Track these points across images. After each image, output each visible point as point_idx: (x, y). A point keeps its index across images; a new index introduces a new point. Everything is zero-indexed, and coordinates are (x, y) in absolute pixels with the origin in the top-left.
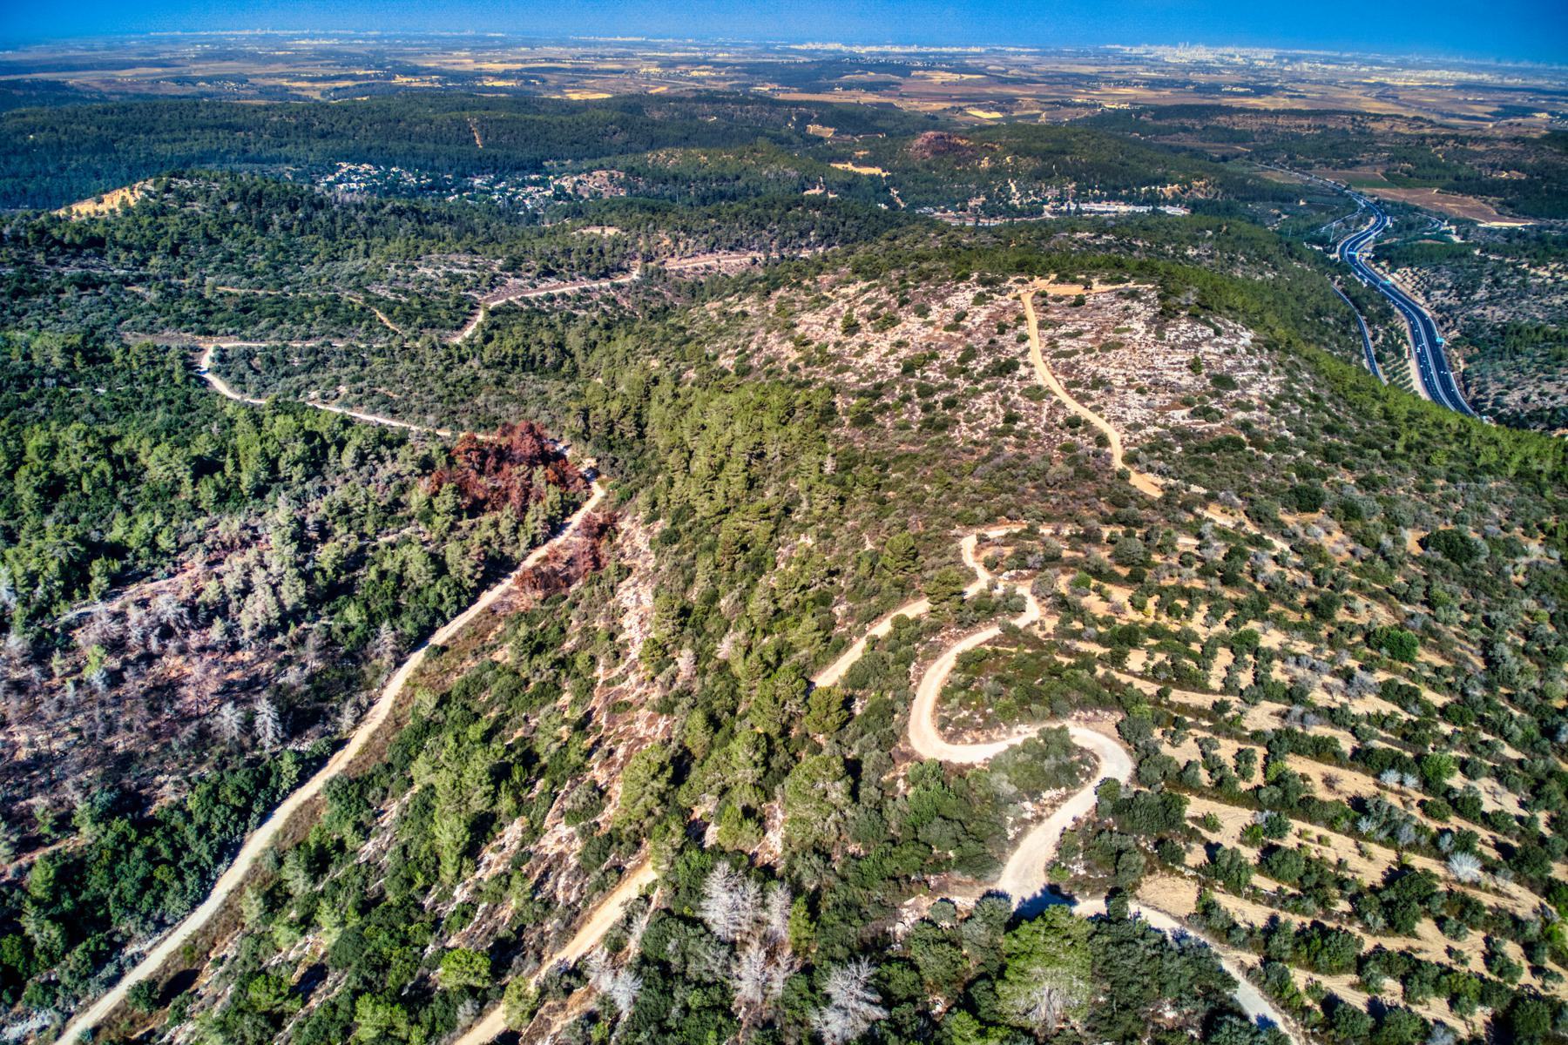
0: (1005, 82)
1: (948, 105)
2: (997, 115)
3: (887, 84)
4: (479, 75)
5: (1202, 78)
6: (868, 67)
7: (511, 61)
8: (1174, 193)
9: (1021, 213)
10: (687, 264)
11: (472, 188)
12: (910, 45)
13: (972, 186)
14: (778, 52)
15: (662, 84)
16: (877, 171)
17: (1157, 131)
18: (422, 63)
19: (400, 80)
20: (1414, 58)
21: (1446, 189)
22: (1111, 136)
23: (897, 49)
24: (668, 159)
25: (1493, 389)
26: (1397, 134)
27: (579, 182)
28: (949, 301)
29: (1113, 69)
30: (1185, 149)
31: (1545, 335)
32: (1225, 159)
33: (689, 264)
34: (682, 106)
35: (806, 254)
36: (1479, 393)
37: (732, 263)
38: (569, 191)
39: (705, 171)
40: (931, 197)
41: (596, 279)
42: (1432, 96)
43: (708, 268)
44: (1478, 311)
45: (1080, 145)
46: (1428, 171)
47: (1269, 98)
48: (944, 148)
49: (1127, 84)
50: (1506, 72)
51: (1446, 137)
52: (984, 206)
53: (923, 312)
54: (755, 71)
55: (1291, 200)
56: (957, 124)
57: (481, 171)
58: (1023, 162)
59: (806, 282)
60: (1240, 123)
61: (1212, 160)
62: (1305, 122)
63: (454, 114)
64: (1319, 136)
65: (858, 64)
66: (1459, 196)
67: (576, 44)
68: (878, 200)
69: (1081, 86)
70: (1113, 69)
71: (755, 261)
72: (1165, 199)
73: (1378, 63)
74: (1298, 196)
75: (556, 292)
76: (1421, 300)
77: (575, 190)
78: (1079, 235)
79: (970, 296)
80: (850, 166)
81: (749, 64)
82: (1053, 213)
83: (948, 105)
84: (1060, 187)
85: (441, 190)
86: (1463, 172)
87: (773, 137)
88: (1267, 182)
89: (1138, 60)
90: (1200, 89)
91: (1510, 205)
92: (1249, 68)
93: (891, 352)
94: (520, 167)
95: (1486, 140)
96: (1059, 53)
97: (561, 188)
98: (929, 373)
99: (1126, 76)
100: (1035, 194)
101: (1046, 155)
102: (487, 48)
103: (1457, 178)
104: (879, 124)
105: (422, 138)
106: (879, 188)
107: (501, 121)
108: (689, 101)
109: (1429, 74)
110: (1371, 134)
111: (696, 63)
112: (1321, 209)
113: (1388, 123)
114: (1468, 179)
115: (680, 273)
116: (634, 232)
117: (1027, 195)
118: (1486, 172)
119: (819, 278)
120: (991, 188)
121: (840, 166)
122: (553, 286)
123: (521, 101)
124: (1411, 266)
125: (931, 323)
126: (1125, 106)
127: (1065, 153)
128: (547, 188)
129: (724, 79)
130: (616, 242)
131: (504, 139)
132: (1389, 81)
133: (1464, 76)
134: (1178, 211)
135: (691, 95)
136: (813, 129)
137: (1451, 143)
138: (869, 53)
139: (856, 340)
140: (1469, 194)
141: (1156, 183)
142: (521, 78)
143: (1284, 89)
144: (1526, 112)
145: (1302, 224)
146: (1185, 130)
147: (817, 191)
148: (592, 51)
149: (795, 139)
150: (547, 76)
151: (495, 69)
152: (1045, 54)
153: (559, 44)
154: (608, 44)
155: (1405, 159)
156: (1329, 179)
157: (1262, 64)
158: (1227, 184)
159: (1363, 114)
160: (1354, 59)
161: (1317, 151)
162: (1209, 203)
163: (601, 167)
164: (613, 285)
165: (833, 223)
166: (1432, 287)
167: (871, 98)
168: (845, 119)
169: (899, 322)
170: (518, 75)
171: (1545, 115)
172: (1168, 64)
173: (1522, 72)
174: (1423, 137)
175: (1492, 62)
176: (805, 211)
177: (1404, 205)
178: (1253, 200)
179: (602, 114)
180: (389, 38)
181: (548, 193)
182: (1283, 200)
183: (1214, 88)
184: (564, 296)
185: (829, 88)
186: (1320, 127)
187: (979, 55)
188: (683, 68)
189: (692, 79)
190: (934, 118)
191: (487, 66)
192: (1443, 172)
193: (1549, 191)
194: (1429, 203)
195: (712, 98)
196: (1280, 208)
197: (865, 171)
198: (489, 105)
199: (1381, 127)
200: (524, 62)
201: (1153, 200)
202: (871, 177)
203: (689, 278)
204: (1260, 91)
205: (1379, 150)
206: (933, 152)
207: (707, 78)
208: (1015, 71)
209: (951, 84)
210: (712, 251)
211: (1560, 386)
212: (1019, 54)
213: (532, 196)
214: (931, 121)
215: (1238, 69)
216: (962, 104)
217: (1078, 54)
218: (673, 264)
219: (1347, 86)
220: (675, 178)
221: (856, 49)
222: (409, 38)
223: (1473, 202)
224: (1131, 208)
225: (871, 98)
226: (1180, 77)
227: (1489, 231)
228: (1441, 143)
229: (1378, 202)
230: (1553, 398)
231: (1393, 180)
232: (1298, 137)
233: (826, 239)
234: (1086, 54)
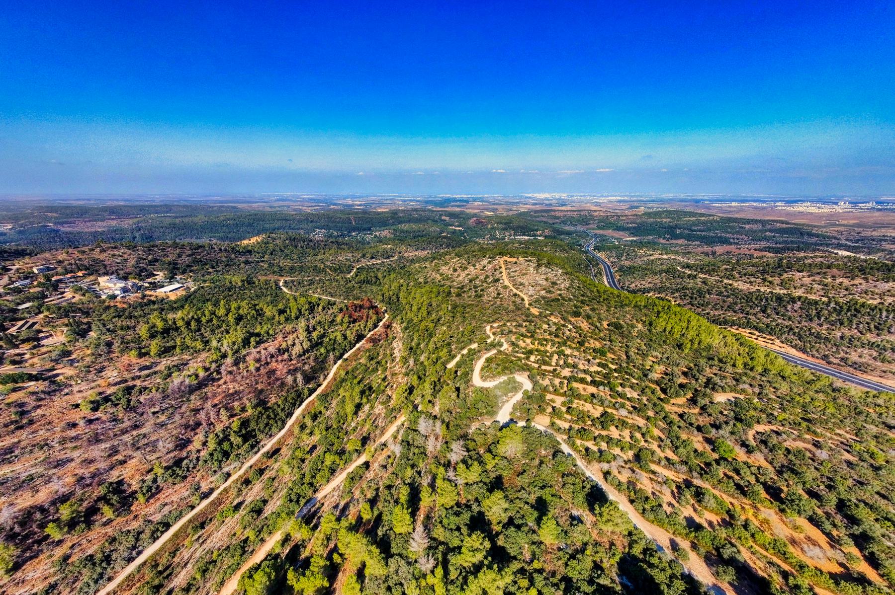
5: (547, 202)
6: (457, 201)
17: (536, 217)
21: (614, 230)
24: (405, 227)
25: (627, 284)
33: (410, 254)
48: (479, 222)
53: (474, 266)
54: (427, 202)
57: (354, 231)
60: (557, 214)
65: (455, 200)
89: (530, 198)
90: (546, 205)
92: (560, 199)
111: (412, 201)
122: (374, 261)
130: (391, 249)
136: (443, 218)
139: (457, 273)
144: (637, 207)
156: (581, 228)
167: (458, 209)
168: (452, 215)
170: (364, 205)
183: (551, 205)
195: (416, 210)
201: (535, 235)
204: (563, 205)
214: (475, 215)
223: (621, 233)
231: (599, 228)
233: (447, 246)
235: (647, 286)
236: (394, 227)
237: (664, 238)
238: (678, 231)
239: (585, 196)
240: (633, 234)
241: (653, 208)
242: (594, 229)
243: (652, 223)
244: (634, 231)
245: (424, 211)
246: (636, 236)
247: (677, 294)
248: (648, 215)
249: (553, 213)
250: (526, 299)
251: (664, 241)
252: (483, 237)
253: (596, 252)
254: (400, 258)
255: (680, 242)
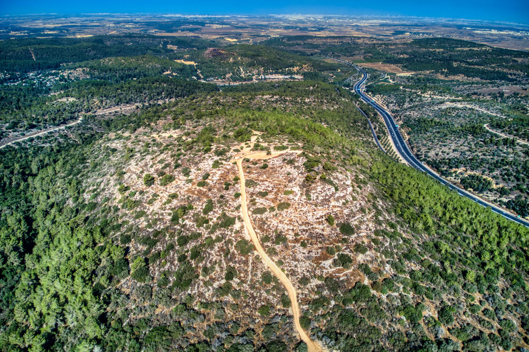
0: (237, 28)
1: (218, 36)
2: (235, 40)
3: (197, 29)
4: (43, 29)
5: (301, 25)
6: (190, 23)
7: (57, 24)
8: (297, 70)
9: (245, 80)
10: (107, 111)
11: (28, 77)
12: (205, 15)
13: (227, 69)
14: (158, 18)
15: (114, 30)
16: (192, 63)
17: (290, 45)
18: (23, 26)
19: (12, 33)
20: (366, 16)
21: (384, 62)
22: (274, 48)
23: (200, 16)
24: (109, 62)
25: (423, 150)
26: (366, 44)
27: (70, 73)
28: (201, 165)
29: (273, 23)
30: (298, 51)
31: (435, 123)
32: (312, 55)
33: (107, 111)
34: (119, 39)
35: (160, 102)
36: (418, 151)
37: (127, 109)
38: (66, 77)
39: (122, 66)
40: (212, 74)
41: (58, 125)
42: (373, 29)
43: (116, 112)
44: (408, 113)
45: (264, 52)
46: (377, 56)
47: (323, 32)
48: (216, 54)
49: (278, 28)
50: (394, 19)
51: (382, 44)
52: (231, 77)
53: (187, 173)
54: (150, 24)
55: (335, 70)
56: (222, 44)
57: (33, 69)
58: (244, 59)
59: (152, 124)
60: (315, 42)
61: (308, 55)
62: (336, 41)
63: (23, 47)
64: (341, 45)
65: (186, 22)
66: (388, 65)
67: (83, 16)
68: (192, 75)
69: (263, 29)
70: (273, 23)
71: (138, 107)
72: (294, 73)
73: (355, 18)
74: (338, 68)
75: (34, 136)
76: (386, 108)
77: (69, 77)
78: (265, 97)
79: (211, 163)
80: (182, 61)
81: (147, 22)
82: (256, 79)
83: (218, 36)
84: (258, 69)
85: (14, 79)
86: (388, 56)
87: (154, 50)
88: (326, 63)
89: (280, 20)
90: (301, 29)
91: (406, 67)
92: (315, 22)
93: (169, 201)
94: (50, 67)
95: (395, 44)
96: (255, 18)
97: (63, 76)
98: (187, 222)
99: (277, 25)
100: (250, 72)
101: (253, 56)
102: (49, 19)
103: (387, 58)
104: (194, 44)
105: (11, 58)
106: (193, 70)
107: (43, 49)
108: (121, 37)
109: (371, 21)
110: (357, 44)
111: (128, 22)
112: (345, 72)
113: (362, 40)
114: (390, 58)
115: (103, 116)
116: (82, 100)
117: (247, 73)
118: (396, 55)
119: (158, 122)
120: (234, 70)
121: (179, 61)
122: (34, 133)
123: (56, 40)
124: (380, 94)
125: (191, 181)
126: (278, 36)
127: (258, 56)
128: (57, 77)
129: (138, 28)
130: (73, 105)
131: (44, 56)
132: (359, 24)
133: (381, 21)
134: (299, 77)
135: (123, 35)
136: (169, 47)
137: (383, 46)
138: (191, 18)
139: (151, 191)
140: (392, 63)
141: (291, 66)
142: (59, 30)
143: (327, 28)
144: (402, 33)
145: (340, 78)
146: (298, 44)
147: (169, 72)
148: (89, 18)
149: (162, 51)
150: (70, 29)
151: (49, 26)
152: (250, 18)
153: (77, 16)
154: (96, 16)
155: (370, 52)
156: (345, 61)
157: (319, 20)
158: (314, 65)
159: (354, 37)
160: (347, 17)
161: (341, 51)
162: (309, 73)
163: (80, 67)
164: (66, 127)
165: (172, 89)
166: (389, 103)
167: (191, 34)
168: (181, 43)
169: (174, 179)
170: (59, 29)
171: (408, 33)
172: (290, 21)
173: (399, 19)
174: (374, 44)
175: (388, 16)
176: (160, 84)
177: (372, 69)
178: (323, 71)
179: (85, 44)
180: (12, 17)
181: (57, 79)
182: (333, 70)
183: (305, 29)
184: (38, 138)
185: (176, 31)
186: (341, 42)
187: (228, 18)
188: (123, 24)
189: (126, 28)
190: (214, 41)
191: (48, 26)
192: (382, 56)
193: (417, 61)
194: (379, 67)
195: (130, 36)
196: (333, 73)
197: (188, 63)
198: (40, 42)
199: (360, 41)
200: (62, 23)
201: (290, 73)
202: (190, 66)
203: (106, 118)
204: (320, 29)
205: (361, 49)
206: (213, 56)
207: (132, 28)
208: (241, 24)
209: (219, 28)
210: (118, 105)
211: (449, 149)
212: (242, 18)
213: (50, 81)
214: (212, 43)
215: (312, 22)
216: (223, 36)
217: (261, 18)
218: (100, 112)
219: (347, 26)
220: (110, 70)
221: (186, 17)
222: (20, 17)
223: (393, 66)
224: (283, 77)
225: (191, 34)
226: (294, 25)
227: (401, 77)
228: (380, 46)
229: (363, 69)
230: (448, 154)
231: (367, 60)
232: (334, 46)
233: (169, 95)
234: (263, 18)
235: (452, 155)
236: (91, 63)
237: (442, 73)
238: (455, 64)
239: (344, 18)
240: (406, 68)
241: (418, 33)
242: (361, 62)
243: (424, 54)
244: (409, 63)
245: (142, 37)
246: (410, 70)
247: (496, 172)
248: (418, 42)
249: (310, 41)
250: (292, 292)
251: (442, 77)
252: (222, 75)
253: (369, 95)
254: (86, 121)
255: (460, 77)
